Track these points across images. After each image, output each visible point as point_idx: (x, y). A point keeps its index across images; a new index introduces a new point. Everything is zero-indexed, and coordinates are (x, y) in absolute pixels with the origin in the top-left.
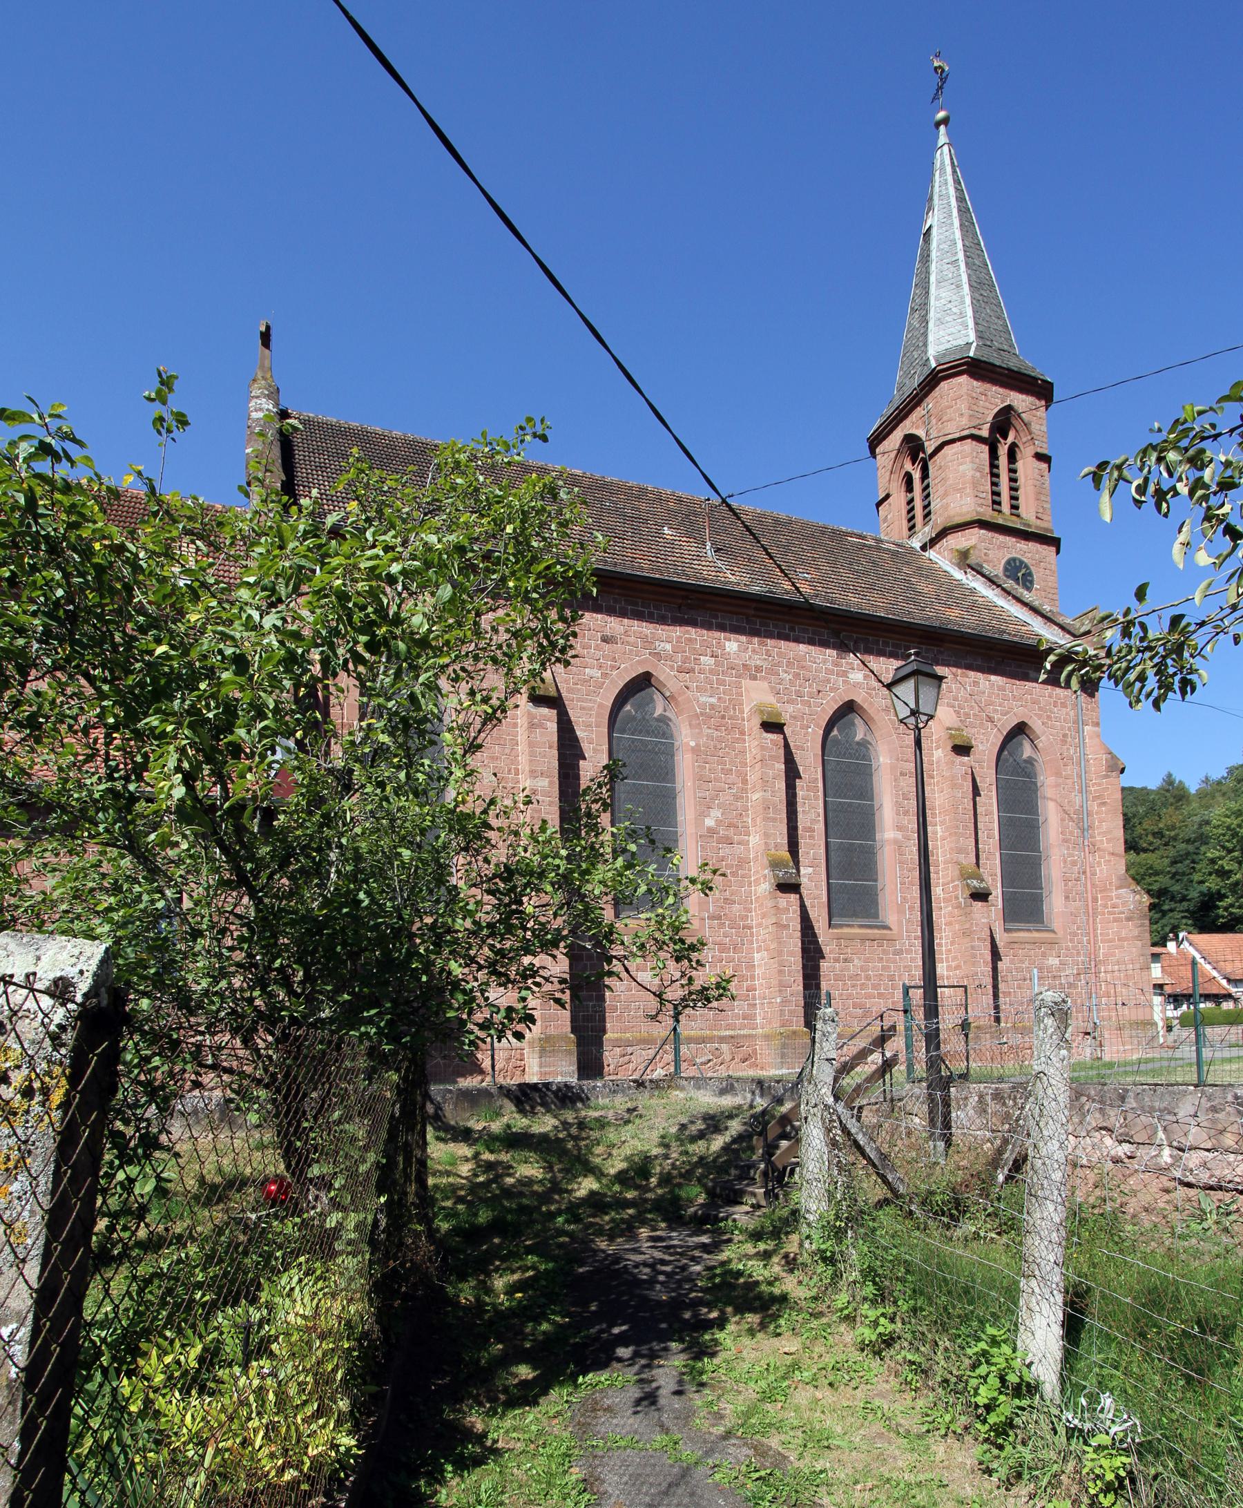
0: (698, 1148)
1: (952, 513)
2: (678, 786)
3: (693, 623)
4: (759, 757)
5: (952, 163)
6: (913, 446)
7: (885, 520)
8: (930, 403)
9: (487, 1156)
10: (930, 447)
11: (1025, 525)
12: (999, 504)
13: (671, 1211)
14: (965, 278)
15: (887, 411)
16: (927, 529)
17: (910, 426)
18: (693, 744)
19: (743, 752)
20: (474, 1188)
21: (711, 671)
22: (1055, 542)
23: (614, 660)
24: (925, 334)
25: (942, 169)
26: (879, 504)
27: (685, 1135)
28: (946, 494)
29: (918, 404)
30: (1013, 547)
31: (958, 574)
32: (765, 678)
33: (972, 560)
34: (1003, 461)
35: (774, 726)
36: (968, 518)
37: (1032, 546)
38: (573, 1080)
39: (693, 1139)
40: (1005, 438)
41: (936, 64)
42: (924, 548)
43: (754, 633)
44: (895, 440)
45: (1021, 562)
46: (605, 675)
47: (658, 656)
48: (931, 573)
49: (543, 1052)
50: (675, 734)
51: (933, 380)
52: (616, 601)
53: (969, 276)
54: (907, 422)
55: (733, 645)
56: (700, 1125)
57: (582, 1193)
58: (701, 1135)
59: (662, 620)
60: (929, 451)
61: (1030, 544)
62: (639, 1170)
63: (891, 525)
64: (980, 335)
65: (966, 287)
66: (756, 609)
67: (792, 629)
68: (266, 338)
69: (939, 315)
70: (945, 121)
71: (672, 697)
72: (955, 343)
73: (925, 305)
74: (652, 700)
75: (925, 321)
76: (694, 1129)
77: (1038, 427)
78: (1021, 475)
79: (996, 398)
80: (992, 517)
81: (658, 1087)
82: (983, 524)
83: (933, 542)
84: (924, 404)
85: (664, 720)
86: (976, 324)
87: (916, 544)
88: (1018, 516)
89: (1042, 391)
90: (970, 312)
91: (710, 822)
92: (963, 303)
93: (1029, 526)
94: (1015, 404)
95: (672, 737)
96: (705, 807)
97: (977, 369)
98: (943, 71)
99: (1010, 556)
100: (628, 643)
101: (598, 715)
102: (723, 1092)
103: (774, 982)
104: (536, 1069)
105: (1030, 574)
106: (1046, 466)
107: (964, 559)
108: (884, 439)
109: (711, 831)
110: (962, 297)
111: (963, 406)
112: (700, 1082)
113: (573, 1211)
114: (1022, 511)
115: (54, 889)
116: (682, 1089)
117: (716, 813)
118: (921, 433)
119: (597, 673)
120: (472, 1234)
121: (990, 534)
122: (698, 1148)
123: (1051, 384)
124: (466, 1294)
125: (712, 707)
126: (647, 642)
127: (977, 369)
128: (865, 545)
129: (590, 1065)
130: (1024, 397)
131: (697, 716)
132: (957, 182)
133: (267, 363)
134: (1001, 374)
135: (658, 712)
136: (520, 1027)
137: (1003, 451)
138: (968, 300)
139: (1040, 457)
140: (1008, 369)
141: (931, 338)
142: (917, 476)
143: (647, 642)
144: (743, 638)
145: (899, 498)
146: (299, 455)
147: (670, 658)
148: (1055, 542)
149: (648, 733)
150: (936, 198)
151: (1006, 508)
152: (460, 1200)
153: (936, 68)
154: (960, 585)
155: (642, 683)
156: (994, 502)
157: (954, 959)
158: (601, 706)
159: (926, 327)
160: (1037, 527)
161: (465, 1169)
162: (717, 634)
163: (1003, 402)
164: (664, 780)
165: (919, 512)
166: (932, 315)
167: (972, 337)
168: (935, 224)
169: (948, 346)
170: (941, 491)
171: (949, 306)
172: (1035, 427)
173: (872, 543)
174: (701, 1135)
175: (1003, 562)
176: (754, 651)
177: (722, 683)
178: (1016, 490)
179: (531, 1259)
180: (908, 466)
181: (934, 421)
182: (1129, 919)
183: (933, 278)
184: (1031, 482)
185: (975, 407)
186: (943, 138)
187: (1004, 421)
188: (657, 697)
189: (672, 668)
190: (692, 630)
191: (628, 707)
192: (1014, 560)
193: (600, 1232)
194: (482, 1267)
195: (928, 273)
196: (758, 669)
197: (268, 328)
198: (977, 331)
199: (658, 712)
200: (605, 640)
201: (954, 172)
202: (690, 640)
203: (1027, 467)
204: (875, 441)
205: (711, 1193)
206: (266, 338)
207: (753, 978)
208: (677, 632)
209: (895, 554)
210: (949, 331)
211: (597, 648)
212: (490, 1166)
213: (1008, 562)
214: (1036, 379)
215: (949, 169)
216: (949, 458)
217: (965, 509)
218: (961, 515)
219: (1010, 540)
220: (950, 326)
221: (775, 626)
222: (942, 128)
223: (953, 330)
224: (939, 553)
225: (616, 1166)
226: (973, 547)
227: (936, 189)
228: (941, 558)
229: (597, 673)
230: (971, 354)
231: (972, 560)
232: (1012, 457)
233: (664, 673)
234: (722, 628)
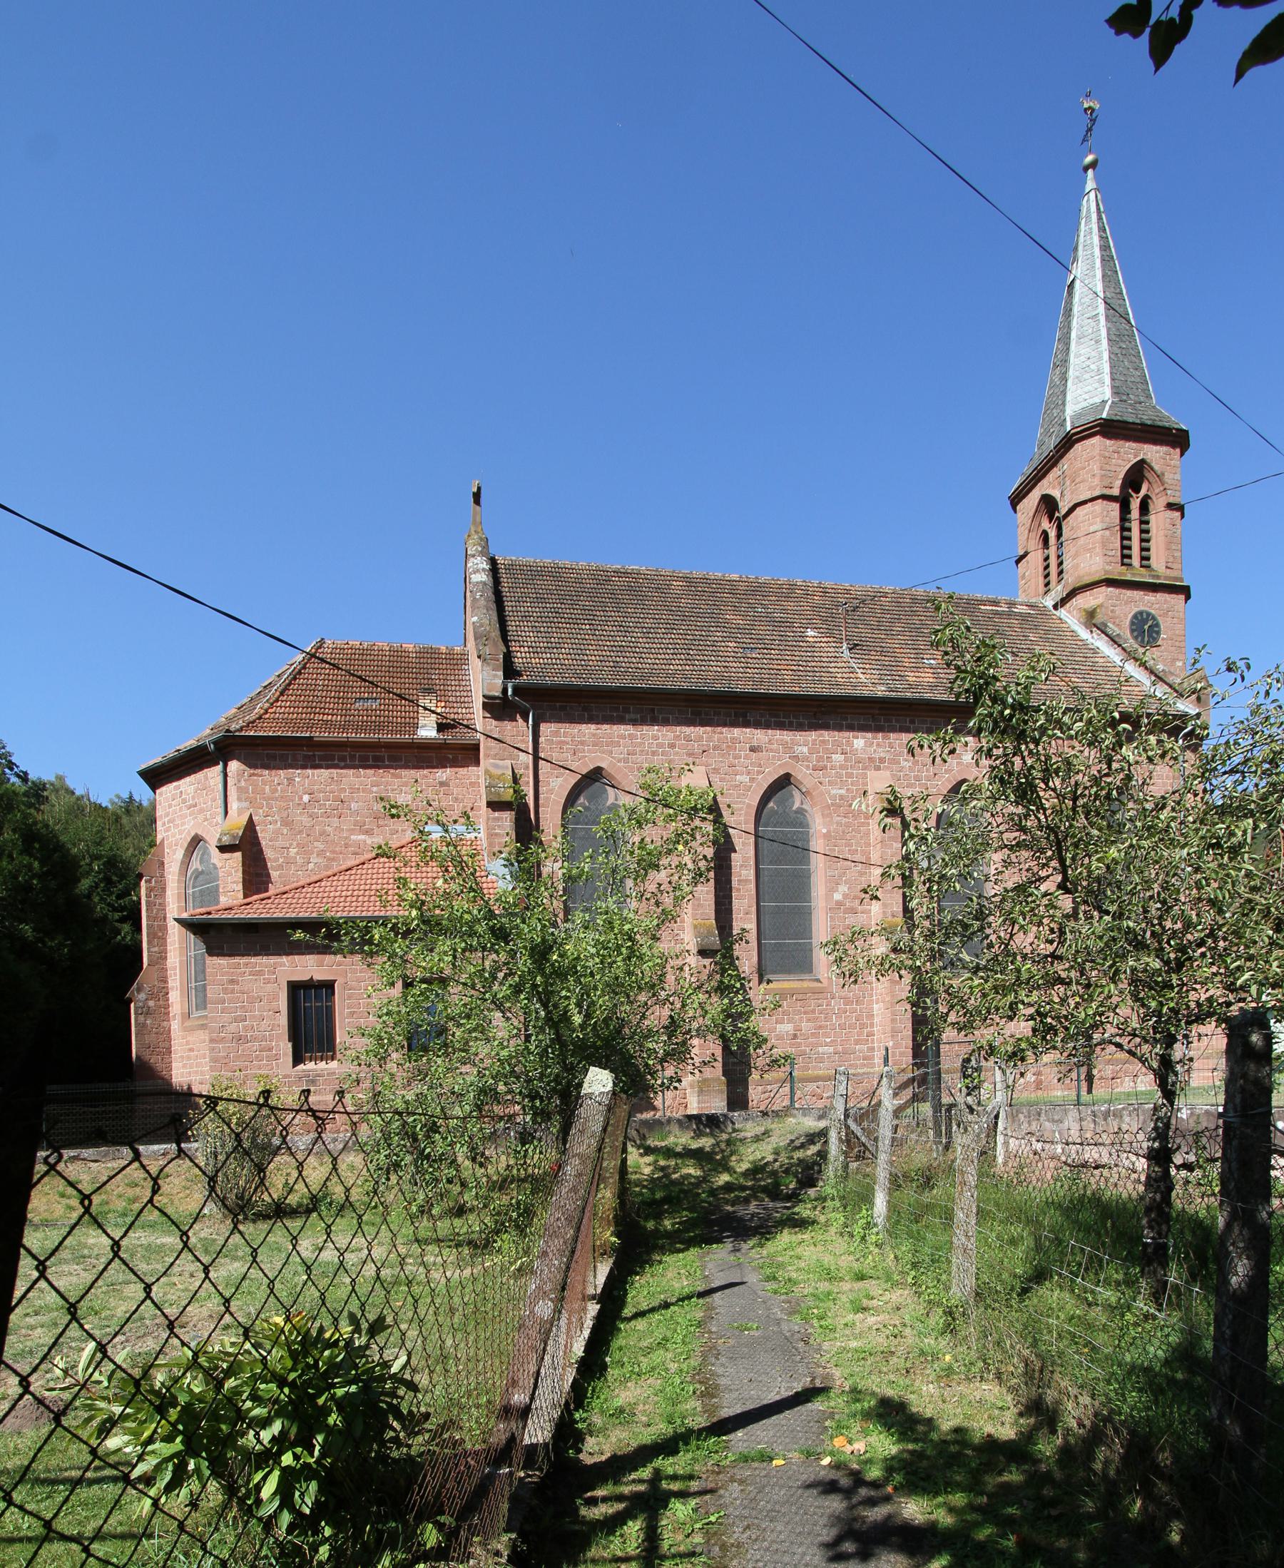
0: (799, 1154)
1: (1082, 572)
2: (812, 867)
3: (826, 727)
4: (879, 839)
5: (1098, 209)
6: (1049, 504)
7: (1023, 577)
8: (1065, 464)
9: (662, 1163)
10: (1064, 508)
11: (1154, 577)
12: (1130, 557)
13: (774, 1193)
14: (1104, 333)
15: (1027, 469)
16: (1059, 588)
17: (1047, 486)
18: (824, 831)
19: (868, 834)
20: (652, 1180)
21: (842, 767)
22: (1185, 591)
23: (760, 766)
24: (1064, 393)
25: (1088, 217)
26: (1018, 562)
27: (793, 1146)
28: (1076, 556)
29: (1054, 465)
30: (1141, 600)
31: (1084, 633)
32: (888, 768)
33: (1099, 619)
34: (1135, 513)
36: (1097, 578)
37: (1161, 597)
39: (798, 1148)
40: (1137, 491)
41: (1086, 106)
42: (1055, 607)
43: (878, 729)
44: (1035, 495)
45: (1149, 614)
46: (752, 780)
47: (796, 758)
48: (1056, 634)
49: (701, 1092)
50: (811, 823)
51: (1068, 443)
52: (762, 716)
53: (1108, 330)
54: (1045, 482)
55: (860, 742)
56: (802, 1140)
57: (721, 1183)
58: (802, 1146)
59: (800, 727)
60: (1063, 511)
61: (1159, 595)
62: (757, 1170)
63: (1027, 587)
64: (1116, 391)
65: (1105, 342)
66: (880, 709)
67: (912, 722)
68: (477, 497)
69: (1077, 374)
70: (1093, 165)
71: (808, 792)
72: (1091, 401)
73: (1065, 361)
74: (792, 796)
75: (1064, 379)
76: (797, 1143)
77: (1171, 476)
78: (1153, 526)
79: (1129, 453)
80: (1120, 574)
81: (777, 1115)
82: (1110, 582)
83: (1063, 602)
84: (1060, 465)
85: (801, 811)
86: (1113, 379)
87: (1049, 602)
88: (1148, 567)
89: (1178, 440)
90: (1107, 369)
91: (837, 896)
92: (1101, 358)
93: (1158, 577)
94: (1148, 457)
95: (807, 826)
96: (833, 884)
97: (1111, 429)
98: (1093, 110)
99: (1137, 610)
100: (772, 750)
101: (746, 814)
102: (821, 1118)
103: (888, 1029)
104: (695, 1105)
105: (1157, 625)
106: (1178, 514)
107: (1090, 618)
108: (1024, 497)
109: (839, 903)
110: (1100, 353)
111: (1095, 467)
112: (806, 1111)
113: (713, 1192)
114: (1153, 562)
116: (794, 1116)
117: (843, 888)
118: (1056, 493)
119: (745, 779)
120: (653, 1203)
121: (1117, 591)
122: (799, 1154)
123: (1186, 432)
124: (650, 1225)
125: (842, 797)
126: (788, 748)
127: (1111, 429)
128: (997, 613)
129: (738, 1100)
130: (1158, 448)
131: (828, 807)
132: (1102, 229)
133: (478, 519)
134: (1135, 430)
135: (797, 805)
136: (676, 1084)
137: (1135, 504)
138: (1106, 356)
139: (1170, 506)
140: (1142, 424)
141: (1069, 398)
142: (1052, 534)
143: (788, 748)
144: (869, 735)
145: (1036, 558)
146: (509, 606)
147: (807, 759)
148: (1185, 591)
149: (788, 824)
150: (1080, 248)
151: (1136, 561)
152: (644, 1187)
153: (1086, 110)
154: (1085, 644)
155: (784, 783)
156: (1123, 556)
158: (749, 806)
159: (1065, 385)
160: (1166, 578)
161: (647, 1170)
162: (846, 734)
163: (1136, 456)
164: (801, 863)
165: (1053, 570)
166: (1072, 374)
167: (1107, 394)
169: (1085, 404)
170: (1073, 551)
171: (1088, 363)
172: (1168, 477)
173: (1004, 608)
174: (802, 1146)
175: (1130, 616)
176: (878, 745)
177: (850, 775)
178: (1148, 541)
179: (685, 1213)
180: (1045, 525)
181: (1068, 483)
183: (1073, 335)
184: (1161, 533)
185: (1108, 467)
186: (1090, 184)
187: (1136, 476)
188: (796, 793)
189: (808, 767)
190: (825, 733)
191: (771, 804)
192: (1141, 613)
193: (727, 1202)
194: (658, 1217)
195: (1069, 328)
196: (882, 760)
197: (479, 488)
198: (1113, 387)
199: (797, 805)
200: (753, 750)
201: (1100, 218)
202: (823, 742)
203: (1160, 520)
204: (1015, 500)
205: (799, 1182)
206: (477, 497)
207: (872, 1025)
208: (813, 735)
209: (1024, 618)
210: (1086, 389)
211: (746, 757)
212: (663, 1169)
213: (1135, 617)
214: (1169, 429)
215: (1094, 217)
216: (1080, 519)
217: (1094, 568)
218: (1090, 574)
219: (1137, 594)
220: (1088, 387)
221: (897, 721)
222: (1090, 172)
223: (1090, 388)
224: (1069, 612)
225: (745, 1166)
226: (1100, 606)
227: (1081, 239)
228: (1070, 618)
229: (745, 779)
230: (1104, 416)
231: (1099, 619)
232: (1144, 507)
233: (802, 773)
234: (851, 728)
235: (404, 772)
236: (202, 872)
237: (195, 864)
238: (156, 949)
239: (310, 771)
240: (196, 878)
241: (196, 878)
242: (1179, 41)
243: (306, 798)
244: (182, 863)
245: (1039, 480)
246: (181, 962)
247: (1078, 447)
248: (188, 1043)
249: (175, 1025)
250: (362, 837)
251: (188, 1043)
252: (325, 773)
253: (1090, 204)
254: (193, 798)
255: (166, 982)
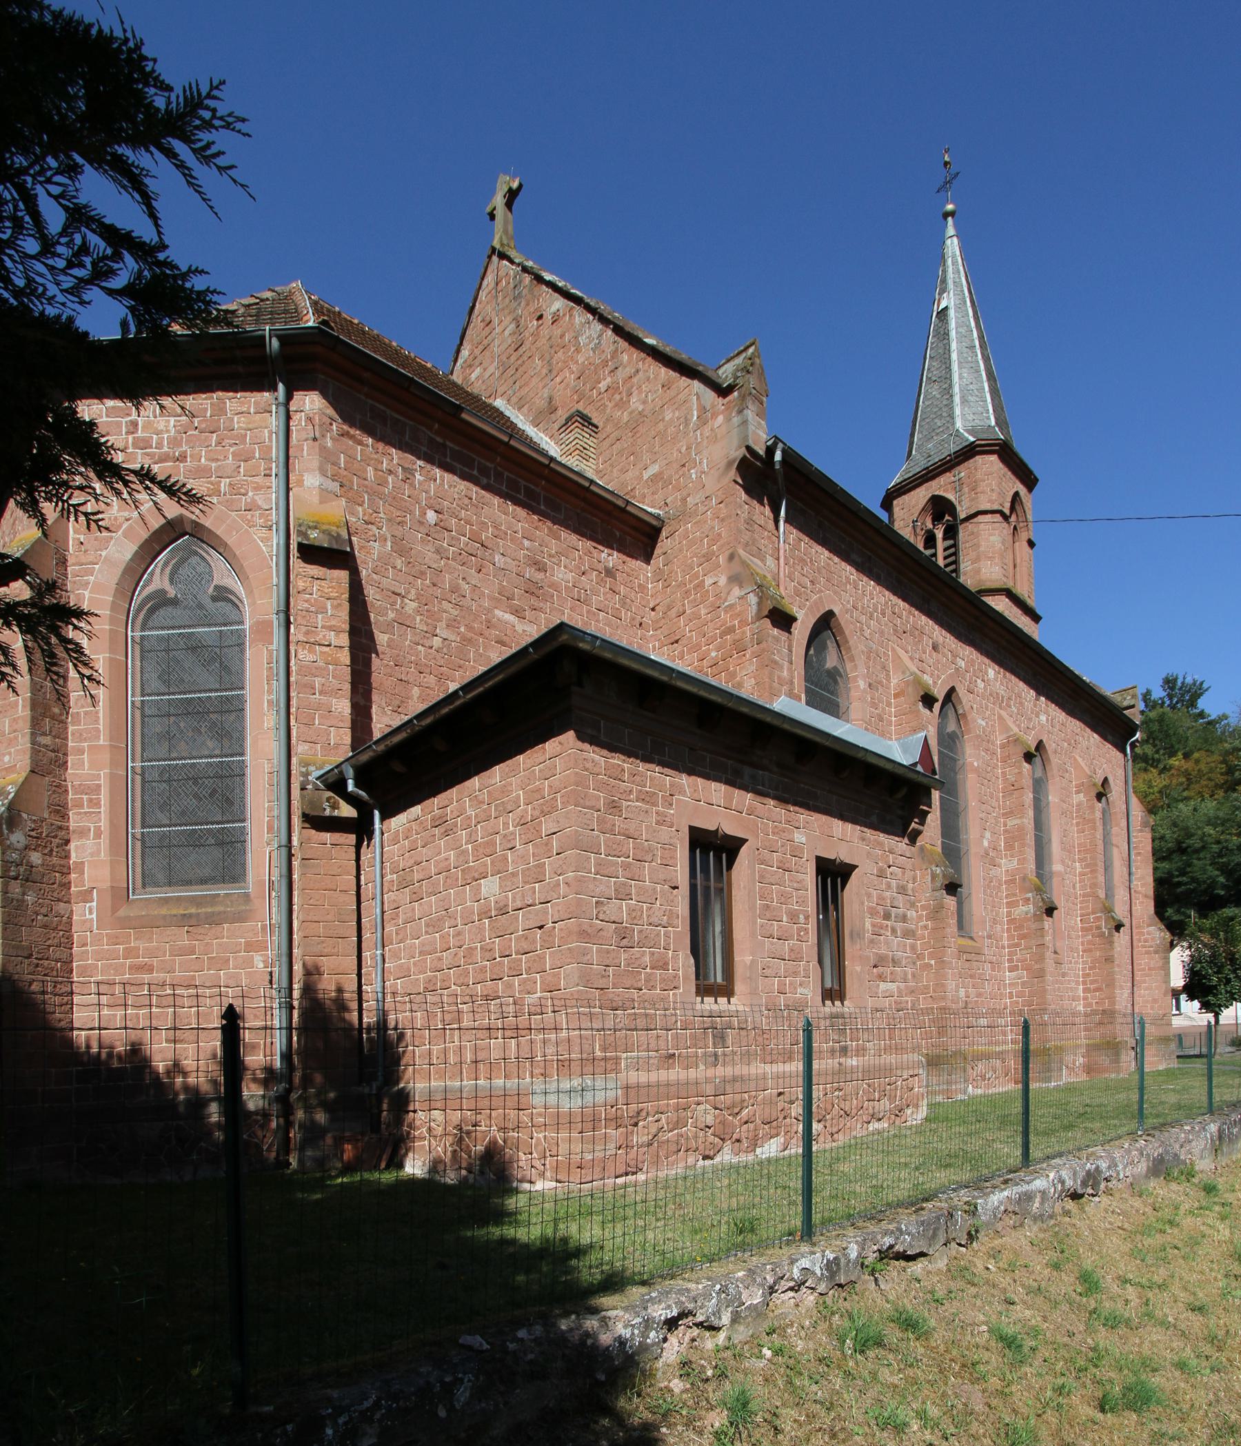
1: (983, 577)
17: (940, 486)
29: (949, 469)
35: (331, 555)
38: (215, 583)
70: (952, 214)
84: (956, 471)
108: (904, 493)
115: (559, 1121)
157: (1092, 982)
168: (952, 305)
170: (973, 555)
182: (1156, 952)
186: (951, 230)
217: (994, 577)
220: (970, 410)
222: (950, 219)
235: (564, 534)
236: (174, 602)
237: (158, 579)
238: (46, 740)
239: (438, 472)
240: (152, 611)
241: (152, 611)
242: (117, 230)
243: (431, 516)
244: (128, 570)
245: (927, 481)
246: (112, 777)
247: (978, 458)
248: (129, 953)
249: (86, 915)
250: (508, 617)
251: (129, 953)
252: (463, 486)
253: (953, 246)
254: (175, 442)
255: (65, 817)
